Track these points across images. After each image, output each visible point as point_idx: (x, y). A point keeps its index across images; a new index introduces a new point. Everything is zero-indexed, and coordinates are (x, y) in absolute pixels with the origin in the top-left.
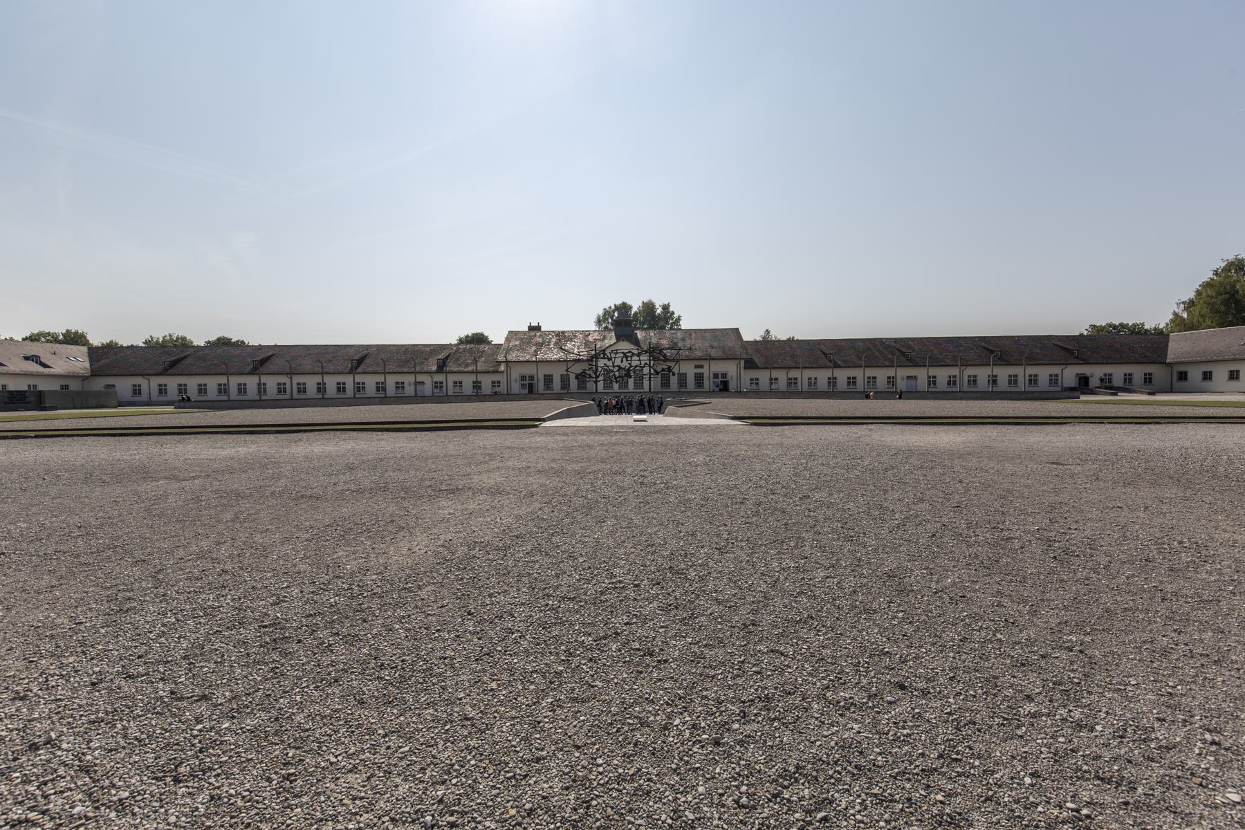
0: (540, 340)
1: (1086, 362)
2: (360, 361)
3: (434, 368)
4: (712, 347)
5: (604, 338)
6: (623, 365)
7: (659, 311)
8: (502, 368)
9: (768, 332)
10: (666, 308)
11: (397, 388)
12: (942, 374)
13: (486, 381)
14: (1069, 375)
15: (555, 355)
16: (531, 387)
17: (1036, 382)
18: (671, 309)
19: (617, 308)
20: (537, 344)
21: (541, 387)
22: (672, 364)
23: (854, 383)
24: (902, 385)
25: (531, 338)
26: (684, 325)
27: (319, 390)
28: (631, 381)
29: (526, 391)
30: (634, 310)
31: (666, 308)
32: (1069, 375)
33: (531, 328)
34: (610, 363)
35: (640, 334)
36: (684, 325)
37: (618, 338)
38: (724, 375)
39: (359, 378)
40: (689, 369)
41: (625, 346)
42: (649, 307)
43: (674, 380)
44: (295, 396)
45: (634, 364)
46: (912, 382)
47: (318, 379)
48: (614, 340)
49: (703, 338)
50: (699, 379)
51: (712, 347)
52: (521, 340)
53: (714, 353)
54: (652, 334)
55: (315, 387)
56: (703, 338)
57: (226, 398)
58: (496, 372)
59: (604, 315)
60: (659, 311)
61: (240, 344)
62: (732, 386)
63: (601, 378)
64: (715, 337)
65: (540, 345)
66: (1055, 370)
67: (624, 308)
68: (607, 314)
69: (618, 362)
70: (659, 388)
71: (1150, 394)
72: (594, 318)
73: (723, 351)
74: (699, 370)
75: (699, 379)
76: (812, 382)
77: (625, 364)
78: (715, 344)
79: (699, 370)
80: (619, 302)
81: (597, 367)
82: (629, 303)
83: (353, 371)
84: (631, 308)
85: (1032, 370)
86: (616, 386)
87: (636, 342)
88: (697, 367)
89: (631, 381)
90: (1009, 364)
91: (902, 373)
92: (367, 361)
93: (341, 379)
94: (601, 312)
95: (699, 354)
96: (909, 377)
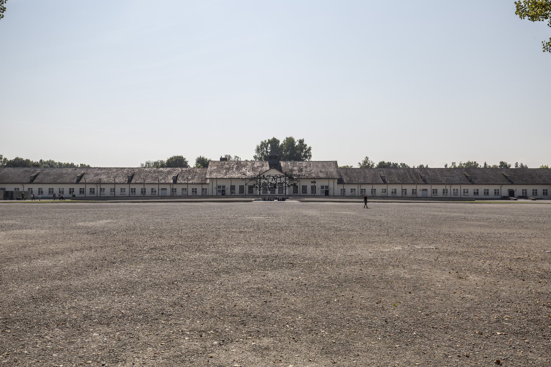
0: (228, 166)
1: (512, 183)
2: (132, 177)
3: (172, 181)
4: (321, 172)
5: (263, 166)
6: (272, 182)
7: (297, 144)
8: (208, 181)
9: (367, 158)
10: (301, 142)
11: (193, 191)
12: (440, 188)
13: (148, 189)
14: (505, 190)
15: (236, 175)
16: (223, 191)
17: (478, 193)
18: (305, 143)
19: (270, 142)
20: (226, 169)
21: (228, 192)
22: (296, 182)
23: (196, 192)
24: (420, 194)
25: (222, 165)
26: (315, 157)
27: (142, 192)
28: (277, 190)
29: (324, 194)
30: (280, 144)
31: (301, 142)
32: (505, 190)
33: (222, 159)
34: (266, 181)
35: (282, 164)
36: (315, 157)
37: (271, 168)
38: (224, 187)
39: (132, 186)
40: (309, 184)
41: (274, 172)
42: (290, 141)
43: (300, 190)
44: (462, 196)
45: (278, 182)
46: (425, 192)
47: (142, 186)
48: (268, 168)
49: (317, 166)
50: (313, 188)
51: (321, 172)
52: (217, 166)
53: (321, 175)
54: (289, 164)
55: (79, 190)
56: (317, 166)
57: (84, 196)
58: (205, 184)
59: (262, 145)
60: (297, 144)
61: (395, 165)
62: (331, 193)
63: (262, 188)
64: (324, 166)
65: (228, 169)
66: (497, 187)
67: (274, 142)
68: (264, 145)
69: (270, 181)
70: (292, 193)
71: (533, 200)
72: (255, 148)
73: (327, 174)
74: (313, 184)
75: (313, 188)
76: (385, 191)
77: (274, 182)
78: (323, 170)
79: (313, 184)
80: (271, 138)
81: (260, 183)
82: (277, 138)
83: (78, 182)
84: (279, 141)
85: (434, 187)
86: (269, 192)
87: (280, 169)
88: (312, 182)
89: (277, 190)
90: (473, 183)
91: (420, 187)
92: (136, 177)
93: (123, 186)
94: (259, 144)
95: (313, 175)
96: (423, 190)
